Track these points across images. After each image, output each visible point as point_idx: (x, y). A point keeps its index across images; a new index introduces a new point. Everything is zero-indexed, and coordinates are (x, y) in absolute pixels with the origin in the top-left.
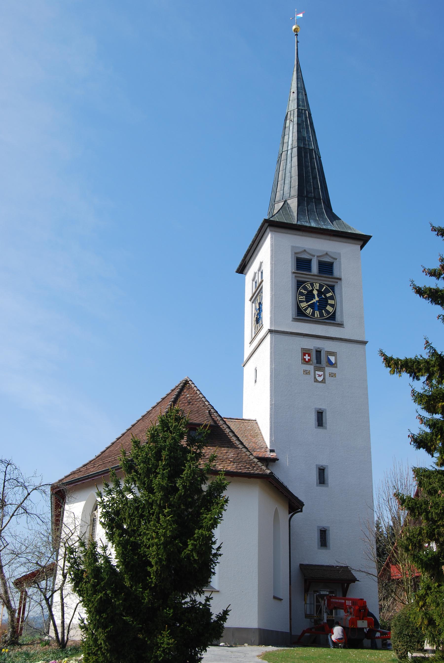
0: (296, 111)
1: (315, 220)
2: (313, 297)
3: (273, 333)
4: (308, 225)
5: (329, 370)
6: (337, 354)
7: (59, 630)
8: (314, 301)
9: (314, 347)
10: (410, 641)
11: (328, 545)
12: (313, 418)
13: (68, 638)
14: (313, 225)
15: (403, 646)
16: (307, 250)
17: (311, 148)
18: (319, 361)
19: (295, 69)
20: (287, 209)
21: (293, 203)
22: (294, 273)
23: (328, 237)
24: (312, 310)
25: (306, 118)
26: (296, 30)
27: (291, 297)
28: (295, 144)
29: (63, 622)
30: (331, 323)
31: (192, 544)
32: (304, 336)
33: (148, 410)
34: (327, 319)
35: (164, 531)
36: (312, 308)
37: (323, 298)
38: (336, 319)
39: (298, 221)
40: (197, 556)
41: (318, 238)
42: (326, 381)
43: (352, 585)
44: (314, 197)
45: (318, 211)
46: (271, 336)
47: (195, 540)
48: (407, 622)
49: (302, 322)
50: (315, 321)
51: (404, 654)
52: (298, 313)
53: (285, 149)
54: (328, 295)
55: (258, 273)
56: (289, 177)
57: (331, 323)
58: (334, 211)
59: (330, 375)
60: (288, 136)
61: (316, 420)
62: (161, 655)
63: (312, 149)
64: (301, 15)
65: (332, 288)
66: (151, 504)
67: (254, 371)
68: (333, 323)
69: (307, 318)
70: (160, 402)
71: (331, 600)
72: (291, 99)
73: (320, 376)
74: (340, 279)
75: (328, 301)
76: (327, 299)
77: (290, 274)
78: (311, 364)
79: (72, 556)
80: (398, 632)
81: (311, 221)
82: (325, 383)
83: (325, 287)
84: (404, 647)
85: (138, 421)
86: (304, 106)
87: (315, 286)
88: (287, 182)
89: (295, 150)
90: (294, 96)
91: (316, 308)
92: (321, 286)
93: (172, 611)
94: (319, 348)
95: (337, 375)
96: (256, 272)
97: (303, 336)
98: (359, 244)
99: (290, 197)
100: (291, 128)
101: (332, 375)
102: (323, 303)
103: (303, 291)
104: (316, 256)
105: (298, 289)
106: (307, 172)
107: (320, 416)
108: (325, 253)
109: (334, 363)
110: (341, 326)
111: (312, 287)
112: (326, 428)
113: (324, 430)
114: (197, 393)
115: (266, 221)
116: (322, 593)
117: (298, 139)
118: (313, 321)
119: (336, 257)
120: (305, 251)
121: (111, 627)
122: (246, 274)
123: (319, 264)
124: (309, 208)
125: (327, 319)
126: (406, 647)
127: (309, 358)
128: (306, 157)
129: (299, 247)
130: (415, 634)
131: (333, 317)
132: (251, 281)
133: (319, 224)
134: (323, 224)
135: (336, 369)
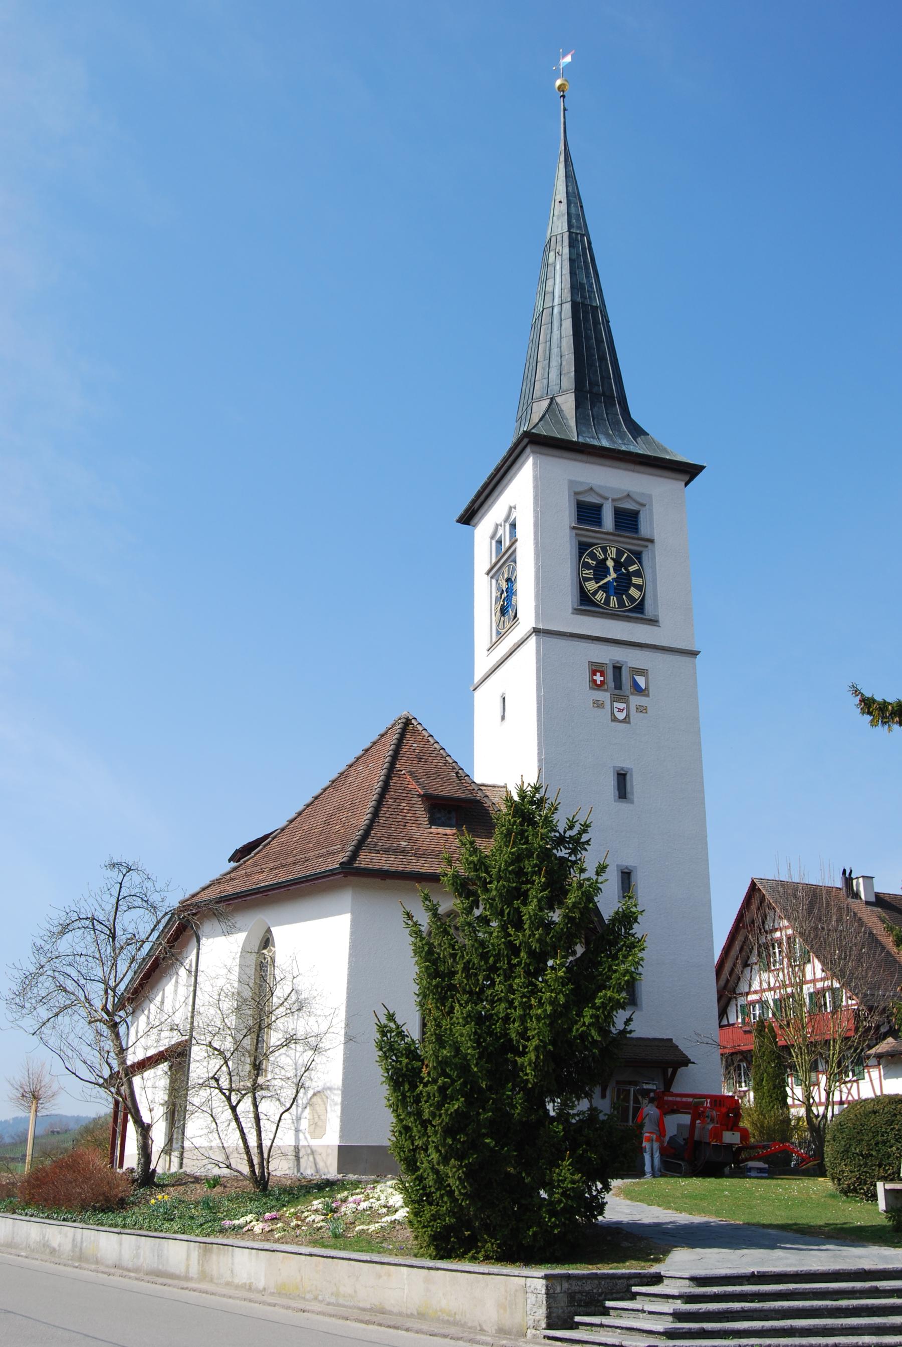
0: (566, 235)
1: (608, 436)
2: (606, 572)
3: (541, 634)
4: (596, 443)
5: (636, 700)
6: (649, 673)
7: (256, 1161)
8: (609, 578)
9: (610, 660)
10: (866, 1164)
11: (639, 1003)
12: (610, 784)
13: (269, 1174)
14: (605, 443)
15: (851, 1172)
16: (595, 488)
17: (594, 304)
18: (618, 685)
19: (562, 159)
20: (557, 412)
21: (567, 403)
22: (574, 528)
23: (632, 466)
24: (605, 595)
25: (584, 249)
26: (561, 88)
27: (569, 571)
28: (568, 296)
29: (260, 1146)
30: (637, 618)
31: (592, 1016)
32: (593, 640)
33: (341, 770)
34: (629, 611)
35: (553, 995)
36: (604, 592)
37: (623, 574)
38: (646, 612)
39: (580, 437)
40: (599, 1035)
41: (613, 467)
42: (631, 720)
43: (682, 1070)
44: (604, 394)
45: (610, 417)
46: (536, 639)
47: (598, 1009)
48: (858, 1133)
49: (589, 615)
50: (612, 614)
51: (854, 1185)
52: (581, 600)
53: (548, 304)
54: (632, 569)
55: (505, 526)
56: (557, 356)
57: (637, 618)
58: (634, 416)
59: (637, 708)
60: (553, 280)
61: (616, 787)
62: (560, 1201)
63: (597, 307)
64: (568, 59)
65: (638, 555)
66: (515, 951)
67: (500, 700)
68: (642, 619)
69: (597, 609)
70: (361, 757)
71: (666, 1098)
72: (556, 214)
73: (620, 710)
74: (652, 541)
75: (631, 580)
76: (629, 575)
77: (568, 530)
78: (606, 690)
79: (385, 1038)
80: (842, 1150)
81: (600, 437)
82: (629, 722)
83: (626, 555)
84: (853, 1174)
85: (325, 790)
86: (579, 228)
87: (609, 552)
88: (555, 363)
89: (568, 307)
90: (561, 209)
91: (612, 591)
92: (620, 553)
93: (561, 1127)
94: (618, 662)
95: (648, 709)
96: (498, 523)
97: (591, 641)
98: (682, 480)
99: (561, 392)
100: (558, 267)
101: (642, 709)
102: (624, 583)
103: (590, 561)
104: (610, 500)
105: (580, 557)
106: (589, 348)
107: (622, 778)
108: (625, 494)
109: (643, 687)
110: (655, 624)
111: (605, 554)
112: (632, 802)
113: (630, 805)
114: (428, 741)
115: (526, 434)
116: (645, 1086)
117: (573, 287)
118: (608, 614)
119: (644, 502)
120: (591, 489)
121: (475, 1156)
122: (475, 526)
123: (578, 507)
124: (595, 413)
125: (629, 611)
126: (857, 1173)
127: (602, 679)
128: (586, 320)
129: (581, 483)
130: (874, 1153)
131: (640, 607)
132: (489, 540)
133: (614, 442)
134: (620, 442)
135: (647, 699)
